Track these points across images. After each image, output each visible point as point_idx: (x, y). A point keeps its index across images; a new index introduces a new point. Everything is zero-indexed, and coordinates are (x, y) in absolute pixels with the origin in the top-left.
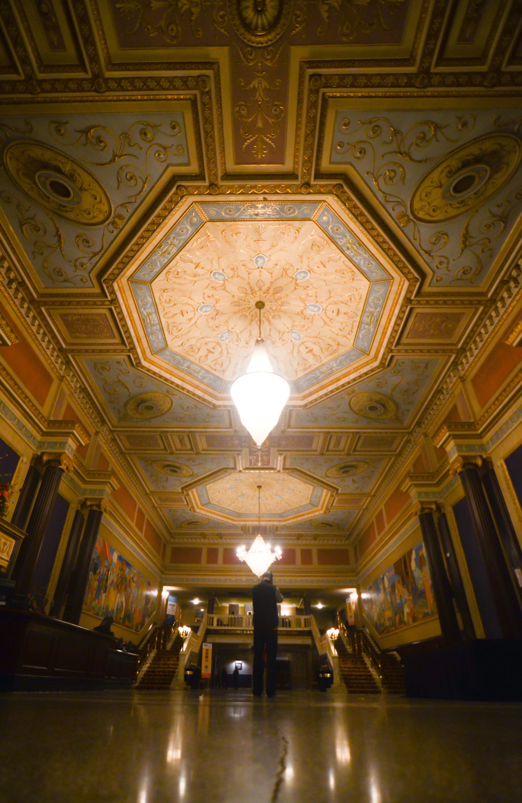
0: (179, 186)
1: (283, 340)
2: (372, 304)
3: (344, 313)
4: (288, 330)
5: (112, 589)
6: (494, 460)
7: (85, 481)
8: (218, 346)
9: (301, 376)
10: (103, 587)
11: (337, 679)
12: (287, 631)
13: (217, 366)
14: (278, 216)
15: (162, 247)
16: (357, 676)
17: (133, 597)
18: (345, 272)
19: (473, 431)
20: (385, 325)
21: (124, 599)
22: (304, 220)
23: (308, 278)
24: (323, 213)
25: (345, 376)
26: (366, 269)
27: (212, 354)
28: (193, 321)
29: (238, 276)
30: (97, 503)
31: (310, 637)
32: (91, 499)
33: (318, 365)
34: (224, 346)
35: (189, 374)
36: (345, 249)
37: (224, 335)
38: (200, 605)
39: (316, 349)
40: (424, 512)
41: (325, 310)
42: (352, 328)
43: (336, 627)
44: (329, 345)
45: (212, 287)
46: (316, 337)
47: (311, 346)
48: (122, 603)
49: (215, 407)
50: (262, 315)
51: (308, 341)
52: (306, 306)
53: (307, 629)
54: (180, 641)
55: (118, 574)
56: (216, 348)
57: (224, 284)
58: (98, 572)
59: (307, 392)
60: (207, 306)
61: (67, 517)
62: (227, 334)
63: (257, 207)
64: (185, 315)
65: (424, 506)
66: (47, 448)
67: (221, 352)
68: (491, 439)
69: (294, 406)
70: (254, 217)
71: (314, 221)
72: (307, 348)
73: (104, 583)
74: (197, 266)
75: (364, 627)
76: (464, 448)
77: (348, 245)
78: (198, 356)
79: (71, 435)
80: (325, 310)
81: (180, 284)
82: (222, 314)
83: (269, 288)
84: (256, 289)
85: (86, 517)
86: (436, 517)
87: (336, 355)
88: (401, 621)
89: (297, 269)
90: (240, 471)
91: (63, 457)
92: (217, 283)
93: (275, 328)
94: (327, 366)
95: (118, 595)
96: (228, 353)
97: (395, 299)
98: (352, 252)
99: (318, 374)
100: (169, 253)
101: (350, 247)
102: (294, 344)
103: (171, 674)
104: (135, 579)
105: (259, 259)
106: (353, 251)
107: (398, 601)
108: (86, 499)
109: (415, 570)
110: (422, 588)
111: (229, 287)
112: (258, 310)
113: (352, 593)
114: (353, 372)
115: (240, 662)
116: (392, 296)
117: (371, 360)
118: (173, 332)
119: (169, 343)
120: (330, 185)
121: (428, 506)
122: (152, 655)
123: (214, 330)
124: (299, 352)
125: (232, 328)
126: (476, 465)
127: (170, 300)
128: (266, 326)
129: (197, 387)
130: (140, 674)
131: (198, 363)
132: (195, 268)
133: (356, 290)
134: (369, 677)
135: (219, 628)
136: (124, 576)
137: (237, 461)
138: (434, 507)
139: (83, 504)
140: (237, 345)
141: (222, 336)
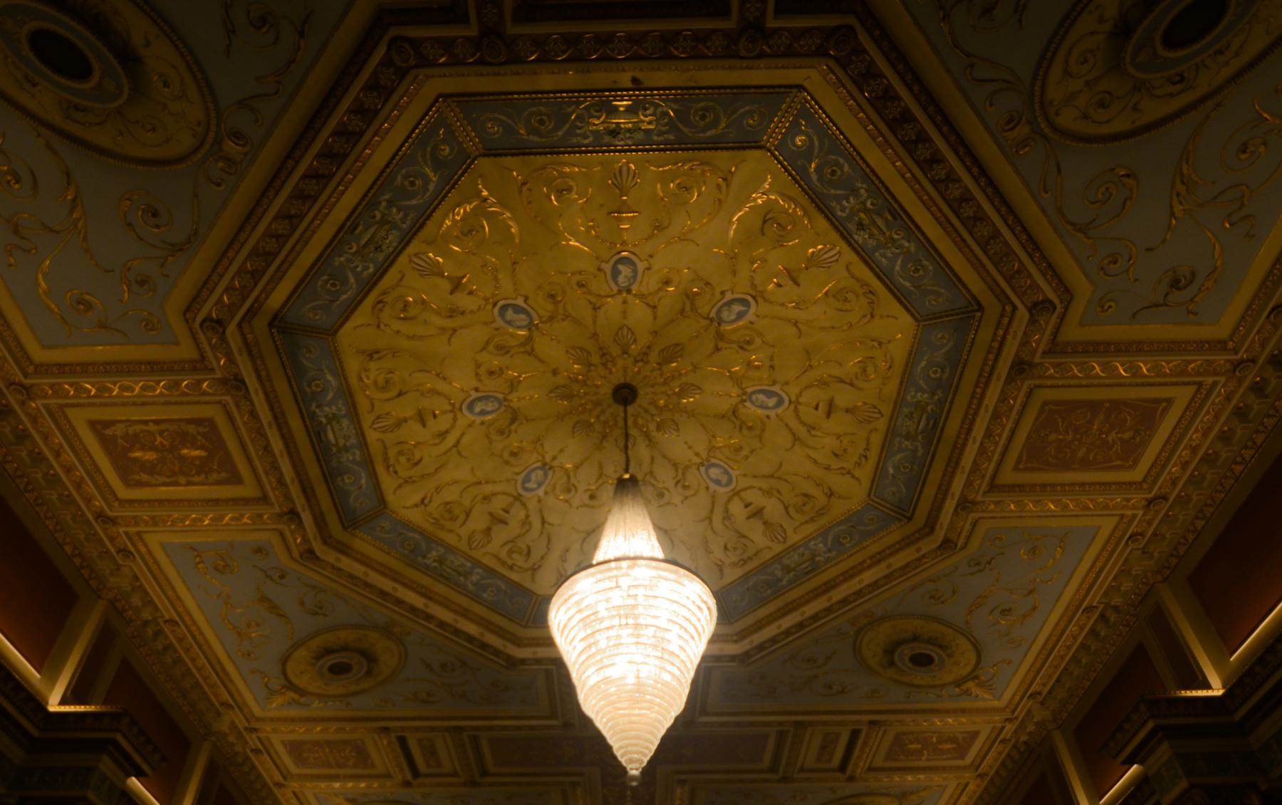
3: (847, 411)
8: (517, 504)
9: (733, 578)
13: (515, 556)
15: (357, 231)
18: (850, 296)
20: (958, 437)
22: (744, 148)
23: (751, 315)
25: (848, 576)
26: (907, 284)
27: (501, 526)
29: (567, 316)
33: (777, 548)
34: (532, 505)
36: (852, 227)
37: (533, 476)
39: (773, 509)
41: (795, 404)
42: (867, 449)
44: (806, 495)
46: (772, 476)
47: (755, 498)
49: (512, 663)
51: (751, 487)
56: (513, 511)
57: (529, 339)
60: (486, 398)
62: (540, 473)
63: (614, 111)
64: (431, 422)
67: (526, 522)
70: (607, 139)
74: (457, 285)
77: (862, 215)
78: (464, 532)
80: (795, 404)
81: (413, 337)
82: (527, 420)
83: (649, 347)
84: (615, 351)
87: (824, 521)
89: (722, 293)
92: (513, 336)
93: (664, 456)
94: (801, 550)
96: (543, 522)
97: (984, 364)
98: (871, 236)
99: (779, 574)
100: (378, 248)
101: (866, 222)
102: (713, 497)
105: (621, 267)
106: (876, 232)
111: (543, 346)
114: (870, 567)
118: (398, 468)
119: (390, 497)
123: (507, 463)
124: (727, 516)
127: (387, 382)
128: (641, 451)
131: (466, 549)
132: (452, 292)
133: (880, 344)
140: (567, 501)
141: (527, 479)
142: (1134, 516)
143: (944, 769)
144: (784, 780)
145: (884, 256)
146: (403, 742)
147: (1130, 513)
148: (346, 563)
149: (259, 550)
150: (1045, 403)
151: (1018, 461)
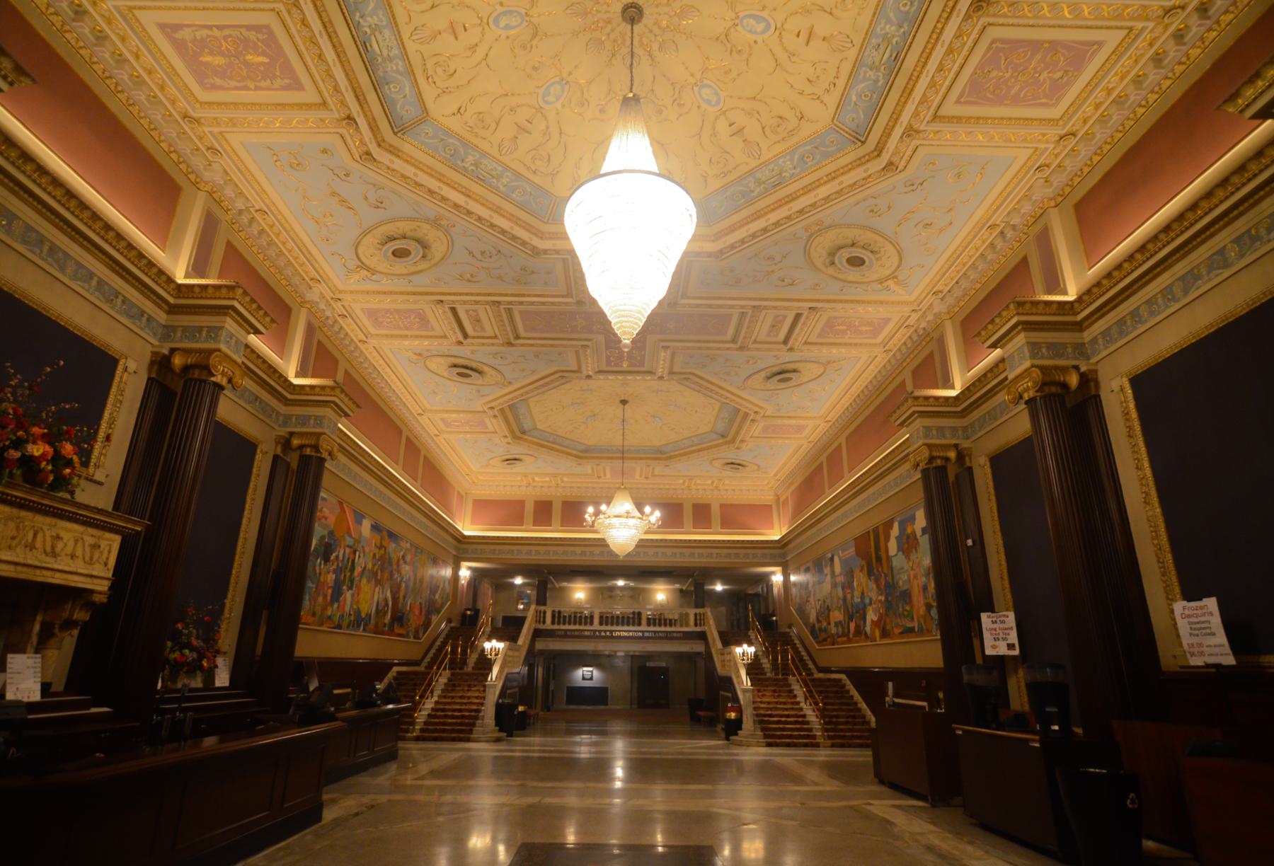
4: (692, 80)
5: (364, 581)
6: (1102, 377)
7: (287, 399)
10: (346, 578)
11: (748, 723)
21: (389, 594)
25: (806, 190)
30: (313, 442)
32: (301, 435)
33: (753, 163)
35: (480, 180)
38: (524, 585)
43: (750, 644)
48: (386, 600)
50: (635, 43)
53: (698, 629)
54: (485, 663)
60: (511, 12)
62: (558, 87)
64: (462, 35)
66: (181, 341)
68: (1106, 333)
75: (790, 627)
85: (294, 465)
86: (952, 472)
88: (859, 632)
90: (589, 377)
91: (213, 360)
99: (752, 186)
104: (408, 558)
107: (857, 600)
108: (291, 434)
113: (773, 573)
118: (436, 79)
119: (431, 106)
122: (442, 680)
125: (570, 74)
126: (1065, 386)
128: (644, 69)
129: (498, 211)
130: (421, 716)
135: (556, 627)
137: (582, 359)
138: (952, 455)
139: (286, 444)
141: (547, 93)
142: (1046, 149)
144: (741, 348)
146: (454, 310)
147: (1042, 146)
148: (398, 164)
151: (961, 96)
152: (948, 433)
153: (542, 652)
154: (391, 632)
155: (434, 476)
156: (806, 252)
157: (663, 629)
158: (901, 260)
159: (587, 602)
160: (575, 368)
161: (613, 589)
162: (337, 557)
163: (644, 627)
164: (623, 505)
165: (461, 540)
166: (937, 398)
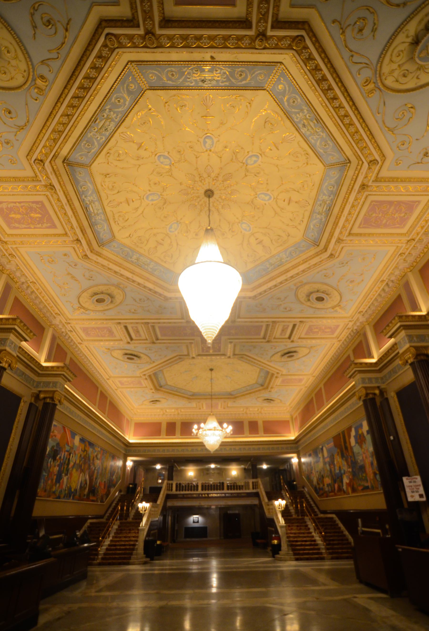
0: (108, 34)
1: (233, 232)
2: (325, 192)
3: (296, 202)
5: (74, 470)
7: (39, 374)
10: (64, 468)
11: (284, 546)
12: (238, 493)
14: (227, 84)
15: (97, 122)
16: (303, 541)
17: (97, 473)
19: (424, 321)
21: (87, 477)
24: (279, 79)
25: (294, 267)
26: (321, 151)
28: (140, 211)
30: (51, 395)
31: (257, 498)
36: (300, 126)
38: (161, 469)
40: (369, 397)
43: (283, 499)
44: (279, 236)
45: (158, 173)
50: (211, 205)
52: (256, 194)
53: (254, 491)
54: (139, 516)
55: (81, 455)
57: (170, 170)
58: (58, 458)
59: (257, 283)
60: (154, 194)
61: (19, 411)
63: (203, 71)
65: (369, 392)
69: (244, 298)
70: (201, 84)
71: (268, 91)
72: (256, 239)
73: (66, 467)
74: (140, 146)
76: (415, 339)
77: (305, 121)
79: (13, 331)
83: (218, 174)
84: (205, 175)
86: (378, 401)
88: (340, 489)
89: (248, 152)
90: (193, 358)
94: (277, 257)
95: (81, 475)
96: (177, 244)
97: (350, 185)
101: (306, 124)
103: (131, 547)
104: (99, 456)
105: (207, 140)
106: (310, 128)
107: (337, 471)
108: (40, 392)
109: (355, 446)
110: (362, 463)
112: (207, 199)
113: (292, 457)
114: (303, 263)
115: (195, 516)
116: (347, 182)
117: (321, 251)
119: (116, 234)
120: (290, 37)
121: (372, 392)
123: (162, 220)
125: (181, 219)
127: (113, 187)
132: (138, 149)
133: (310, 175)
134: (313, 543)
135: (178, 493)
136: (87, 456)
138: (377, 392)
139: (37, 397)
141: (171, 227)
142: (402, 247)
143: (326, 338)
144: (268, 342)
145: (312, 138)
146: (126, 327)
148: (100, 260)
149: (65, 255)
150: (372, 201)
151: (360, 224)
152: (374, 381)
153: (171, 508)
154: (88, 499)
155: (115, 411)
156: (296, 295)
157: (235, 491)
158: (341, 298)
159: (195, 477)
160: (185, 353)
161: (209, 469)
162: (60, 457)
163: (225, 491)
164: (212, 423)
165: (128, 445)
166: (366, 364)
